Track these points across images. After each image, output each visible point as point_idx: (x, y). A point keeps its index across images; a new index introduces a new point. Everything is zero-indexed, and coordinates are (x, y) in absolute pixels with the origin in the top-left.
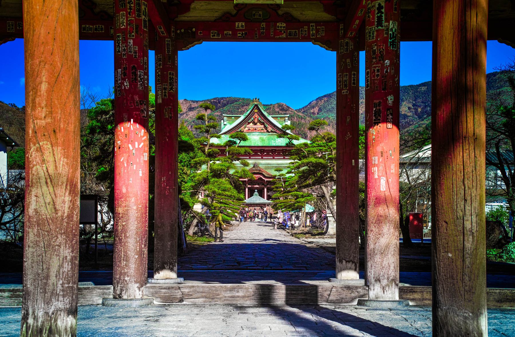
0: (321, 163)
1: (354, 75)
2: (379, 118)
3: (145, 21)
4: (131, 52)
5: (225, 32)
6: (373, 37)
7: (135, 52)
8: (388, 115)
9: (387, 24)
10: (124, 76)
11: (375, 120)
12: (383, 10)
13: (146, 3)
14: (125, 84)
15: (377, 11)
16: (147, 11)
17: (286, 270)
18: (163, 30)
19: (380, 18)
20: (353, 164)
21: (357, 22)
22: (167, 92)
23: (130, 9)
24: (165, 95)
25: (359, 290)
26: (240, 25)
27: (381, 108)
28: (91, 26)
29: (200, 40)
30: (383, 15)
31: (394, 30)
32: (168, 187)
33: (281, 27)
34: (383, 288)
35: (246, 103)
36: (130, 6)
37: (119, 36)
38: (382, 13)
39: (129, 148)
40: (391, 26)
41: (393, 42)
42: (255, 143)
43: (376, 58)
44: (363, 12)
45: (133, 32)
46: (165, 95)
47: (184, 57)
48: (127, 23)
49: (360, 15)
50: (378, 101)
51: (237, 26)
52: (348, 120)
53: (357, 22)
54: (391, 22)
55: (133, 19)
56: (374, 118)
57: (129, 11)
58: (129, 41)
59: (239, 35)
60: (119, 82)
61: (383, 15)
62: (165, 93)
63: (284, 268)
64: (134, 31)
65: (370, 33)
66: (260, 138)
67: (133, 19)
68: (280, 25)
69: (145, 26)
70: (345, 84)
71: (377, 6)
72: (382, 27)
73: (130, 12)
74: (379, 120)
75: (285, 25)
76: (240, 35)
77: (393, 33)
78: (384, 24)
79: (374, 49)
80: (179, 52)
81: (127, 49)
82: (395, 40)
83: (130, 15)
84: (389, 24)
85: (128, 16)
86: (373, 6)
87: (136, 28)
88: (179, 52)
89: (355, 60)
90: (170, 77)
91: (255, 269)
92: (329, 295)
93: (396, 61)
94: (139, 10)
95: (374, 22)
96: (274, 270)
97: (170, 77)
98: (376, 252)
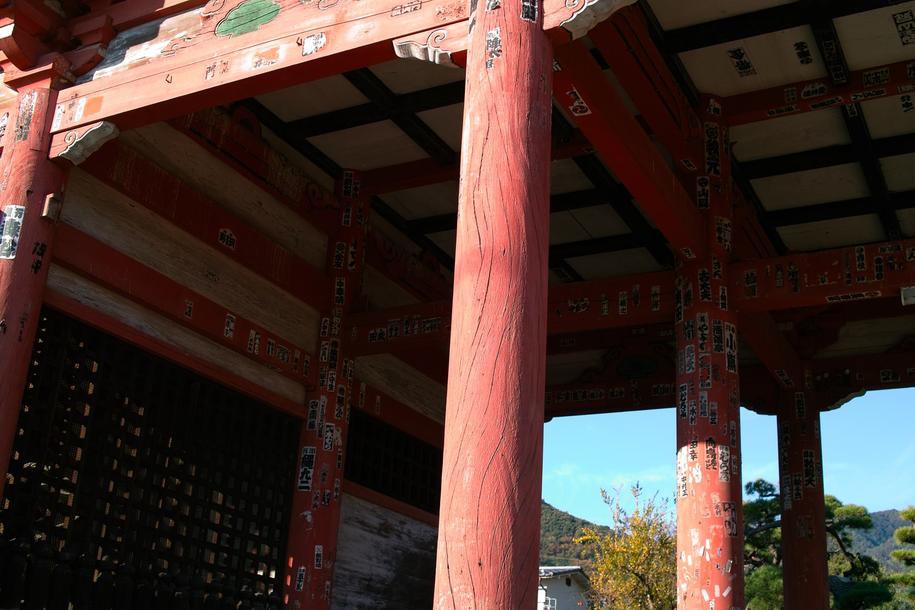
3: (731, 357)
5: (908, 370)
7: (713, 413)
10: (693, 458)
11: (708, 159)
13: (732, 326)
16: (734, 338)
18: (786, 377)
22: (801, 487)
23: (703, 338)
24: (798, 494)
28: (667, 386)
29: (859, 391)
39: (702, 597)
46: (798, 494)
48: (697, 363)
55: (707, 355)
58: (701, 394)
62: (798, 489)
64: (710, 376)
67: (707, 355)
69: (731, 366)
73: (702, 344)
80: (823, 415)
81: (697, 409)
83: (702, 349)
85: (700, 350)
87: (714, 371)
88: (823, 415)
94: (719, 339)
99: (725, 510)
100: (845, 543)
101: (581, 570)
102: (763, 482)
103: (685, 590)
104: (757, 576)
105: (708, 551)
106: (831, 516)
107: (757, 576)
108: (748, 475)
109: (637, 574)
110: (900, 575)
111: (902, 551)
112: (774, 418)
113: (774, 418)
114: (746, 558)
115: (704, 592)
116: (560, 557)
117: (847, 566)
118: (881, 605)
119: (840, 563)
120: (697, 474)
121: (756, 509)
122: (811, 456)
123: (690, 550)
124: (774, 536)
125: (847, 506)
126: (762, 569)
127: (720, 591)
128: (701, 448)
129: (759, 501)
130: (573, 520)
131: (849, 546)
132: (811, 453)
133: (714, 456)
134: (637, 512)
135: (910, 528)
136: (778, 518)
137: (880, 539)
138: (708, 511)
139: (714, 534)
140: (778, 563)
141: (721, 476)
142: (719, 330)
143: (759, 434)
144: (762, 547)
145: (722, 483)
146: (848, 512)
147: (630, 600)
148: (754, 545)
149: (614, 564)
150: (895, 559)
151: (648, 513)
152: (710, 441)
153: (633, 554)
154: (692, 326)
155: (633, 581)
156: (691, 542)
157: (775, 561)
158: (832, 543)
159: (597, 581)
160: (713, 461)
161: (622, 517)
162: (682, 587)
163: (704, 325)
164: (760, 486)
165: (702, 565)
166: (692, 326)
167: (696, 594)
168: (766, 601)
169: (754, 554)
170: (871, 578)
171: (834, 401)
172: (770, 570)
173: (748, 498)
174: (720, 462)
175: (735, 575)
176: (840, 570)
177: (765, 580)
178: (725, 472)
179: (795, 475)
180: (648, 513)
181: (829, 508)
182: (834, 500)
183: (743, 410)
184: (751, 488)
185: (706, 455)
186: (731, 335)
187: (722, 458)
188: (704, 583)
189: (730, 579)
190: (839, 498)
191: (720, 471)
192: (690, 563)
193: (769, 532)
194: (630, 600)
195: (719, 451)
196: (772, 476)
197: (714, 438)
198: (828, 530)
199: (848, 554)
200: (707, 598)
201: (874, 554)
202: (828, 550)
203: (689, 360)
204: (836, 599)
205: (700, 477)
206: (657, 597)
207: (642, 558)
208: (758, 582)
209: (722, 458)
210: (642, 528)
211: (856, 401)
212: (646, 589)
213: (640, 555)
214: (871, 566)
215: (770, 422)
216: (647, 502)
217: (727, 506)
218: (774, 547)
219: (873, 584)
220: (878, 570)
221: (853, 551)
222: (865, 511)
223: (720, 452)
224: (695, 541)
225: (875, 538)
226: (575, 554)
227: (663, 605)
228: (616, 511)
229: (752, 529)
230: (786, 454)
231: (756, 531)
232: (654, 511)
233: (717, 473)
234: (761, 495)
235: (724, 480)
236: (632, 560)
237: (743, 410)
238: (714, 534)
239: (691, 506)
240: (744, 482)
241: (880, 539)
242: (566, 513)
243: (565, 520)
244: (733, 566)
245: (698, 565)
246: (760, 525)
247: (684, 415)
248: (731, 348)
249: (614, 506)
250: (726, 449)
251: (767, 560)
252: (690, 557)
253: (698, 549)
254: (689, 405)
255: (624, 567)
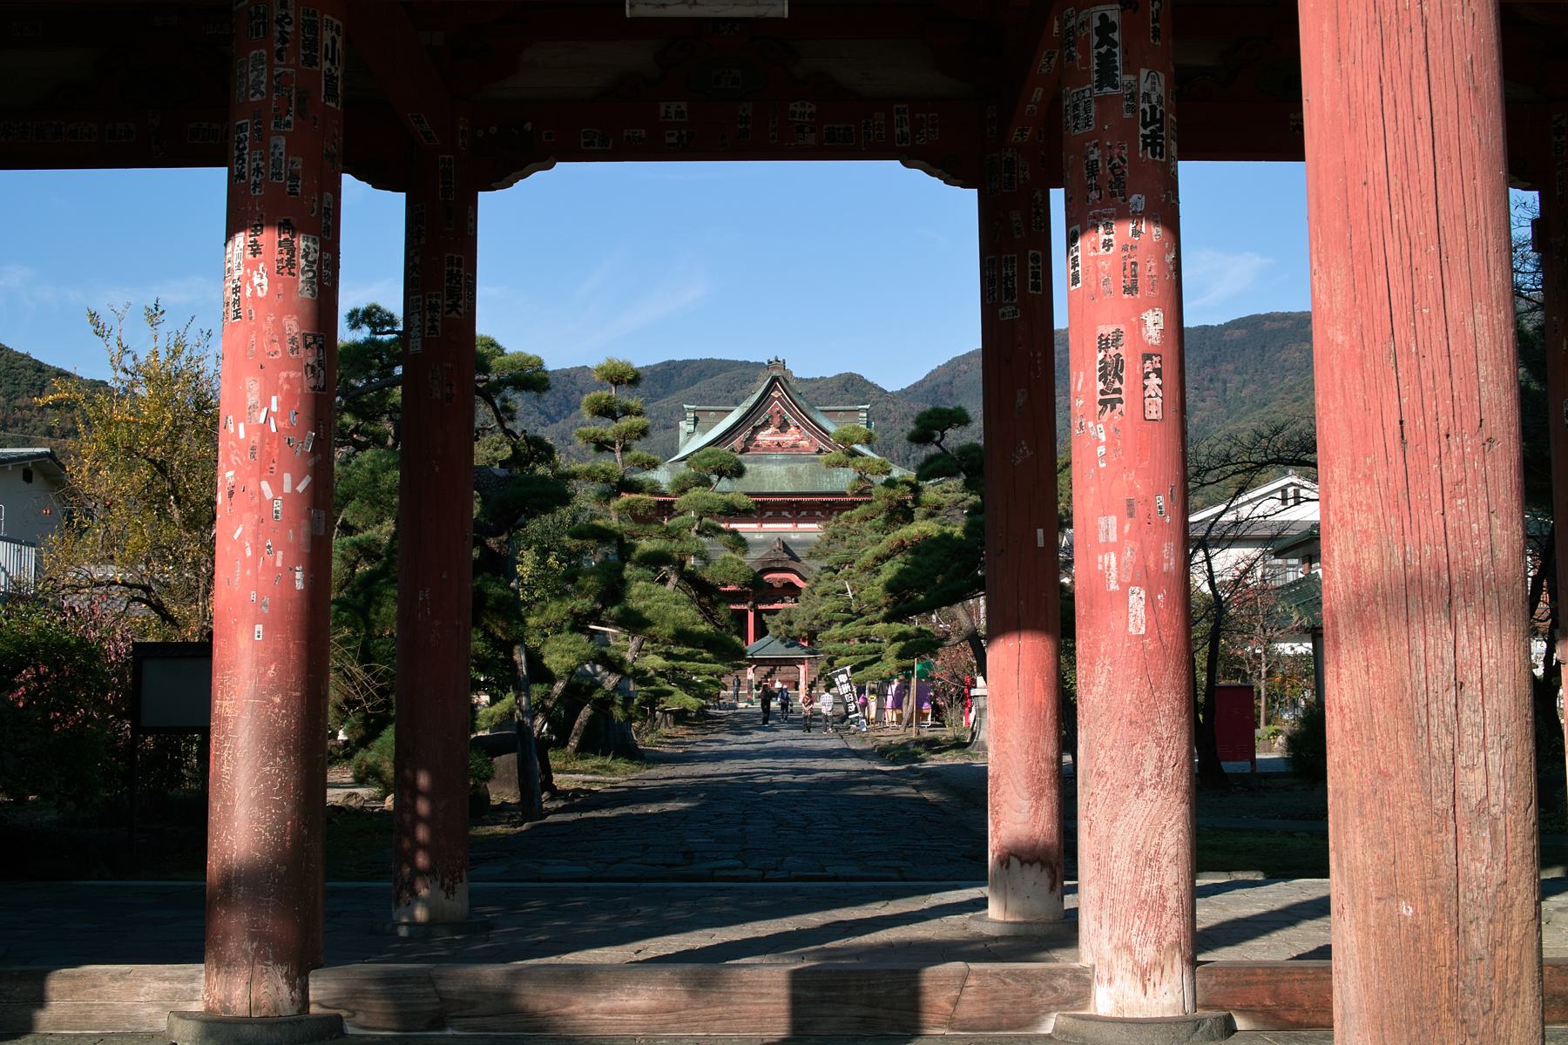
0: (926, 538)
1: (1035, 259)
2: (1117, 385)
3: (331, 78)
4: (278, 175)
5: (626, 133)
6: (1088, 119)
7: (294, 177)
8: (1147, 376)
9: (1132, 78)
10: (254, 254)
11: (1103, 392)
12: (1116, 36)
13: (336, 22)
14: (256, 280)
15: (1096, 39)
16: (339, 46)
17: (836, 879)
19: (1106, 62)
20: (1041, 543)
21: (1038, 93)
22: (438, 317)
23: (283, 40)
24: (433, 328)
25: (1061, 982)
26: (673, 110)
27: (1121, 351)
29: (545, 160)
30: (1116, 50)
31: (1154, 99)
32: (437, 623)
33: (802, 114)
34: (1143, 974)
35: (746, 371)
36: (283, 33)
37: (242, 128)
38: (1115, 44)
39: (261, 493)
40: (1145, 87)
41: (1154, 134)
42: (775, 484)
43: (1098, 188)
44: (1053, 61)
45: (288, 112)
47: (496, 211)
49: (1044, 71)
50: (1111, 329)
51: (663, 113)
52: (1020, 401)
53: (1038, 93)
54: (1144, 72)
55: (290, 70)
56: (1100, 386)
57: (279, 46)
58: (274, 140)
59: (669, 140)
60: (237, 274)
61: (1116, 50)
62: (433, 320)
63: (830, 871)
65: (1076, 107)
66: (789, 470)
67: (290, 70)
68: (798, 109)
69: (331, 94)
70: (1007, 289)
71: (1096, 23)
72: (1115, 87)
73: (281, 50)
74: (1119, 391)
75: (814, 109)
76: (673, 140)
77: (1153, 108)
78: (1124, 78)
79: (1092, 157)
80: (484, 197)
82: (1161, 129)
83: (281, 59)
84: (1138, 80)
86: (1082, 25)
88: (484, 197)
89: (1038, 213)
90: (450, 272)
91: (736, 879)
92: (956, 1002)
93: (1167, 200)
94: (312, 45)
95: (1088, 71)
96: (796, 879)
97: (450, 272)
98: (1117, 848)
99: (307, 346)
100: (505, 414)
101: (51, 455)
102: (378, 309)
103: (231, 481)
104: (359, 465)
105: (275, 415)
106: (486, 369)
107: (359, 465)
108: (350, 298)
109: (152, 461)
110: (585, 466)
111: (592, 429)
112: (401, 197)
113: (401, 197)
114: (343, 436)
115: (265, 486)
116: (14, 433)
117: (506, 452)
118: (553, 512)
119: (496, 449)
120: (261, 281)
121: (360, 355)
122: (459, 264)
123: (243, 415)
124: (391, 401)
125: (513, 355)
126: (369, 453)
127: (293, 484)
128: (270, 238)
129: (368, 342)
130: (40, 368)
131: (511, 419)
132: (459, 260)
133: (292, 251)
134: (156, 353)
135: (606, 393)
136: (399, 370)
137: (560, 412)
138: (277, 347)
139: (286, 387)
140: (395, 445)
141: (302, 287)
142: (313, 27)
143: (374, 222)
144: (372, 418)
145: (304, 299)
146: (513, 365)
147: (142, 504)
148: (357, 415)
149: (112, 443)
150: (580, 442)
151: (175, 355)
152: (285, 226)
153: (146, 426)
154: (264, 15)
155: (145, 472)
156: (245, 400)
157: (390, 442)
158: (483, 414)
159: (78, 473)
160: (289, 260)
161: (128, 362)
162: (227, 476)
163: (287, 16)
164: (370, 316)
165: (262, 439)
166: (264, 15)
167: (251, 487)
168: (372, 505)
169: (356, 430)
170: (541, 470)
171: (502, 177)
172: (380, 456)
173: (346, 335)
174: (303, 262)
175: (319, 456)
176: (495, 460)
177: (372, 472)
178: (310, 281)
179: (431, 296)
180: (175, 355)
181: (484, 357)
182: (493, 344)
183: (347, 180)
184: (356, 319)
185: (277, 249)
186: (333, 39)
187: (305, 256)
188: (265, 470)
189: (310, 463)
190: (500, 342)
191: (302, 278)
192: (242, 435)
193: (383, 395)
194: (142, 504)
195: (301, 243)
196: (393, 302)
197: (294, 221)
198: (479, 392)
199: (508, 433)
200: (269, 494)
201: (549, 435)
202: (477, 425)
203: (256, 78)
204: (484, 503)
205: (265, 288)
206: (187, 499)
207: (162, 433)
208: (361, 475)
209: (305, 256)
210: (162, 381)
211: (538, 176)
212: (168, 486)
213: (158, 427)
214: (543, 451)
215: (394, 204)
216: (174, 337)
217: (310, 340)
218: (391, 419)
219: (544, 478)
220: (552, 458)
221: (517, 426)
222: (540, 363)
223: (303, 245)
224: (252, 399)
225: (553, 411)
226: (43, 429)
227: (198, 512)
228: (117, 350)
229: (354, 388)
230: (417, 260)
231: (362, 392)
232: (186, 352)
233: (296, 282)
234: (374, 332)
235: (307, 294)
236: (144, 438)
237: (347, 180)
238: (286, 387)
239: (247, 338)
240: (344, 308)
241: (560, 412)
242: (27, 356)
243: (25, 367)
244: (316, 441)
245: (255, 438)
246: (369, 382)
247: (241, 176)
248: (333, 63)
249: (113, 341)
250: (314, 241)
251: (378, 440)
252: (241, 426)
253: (256, 414)
254: (251, 160)
255: (130, 450)
